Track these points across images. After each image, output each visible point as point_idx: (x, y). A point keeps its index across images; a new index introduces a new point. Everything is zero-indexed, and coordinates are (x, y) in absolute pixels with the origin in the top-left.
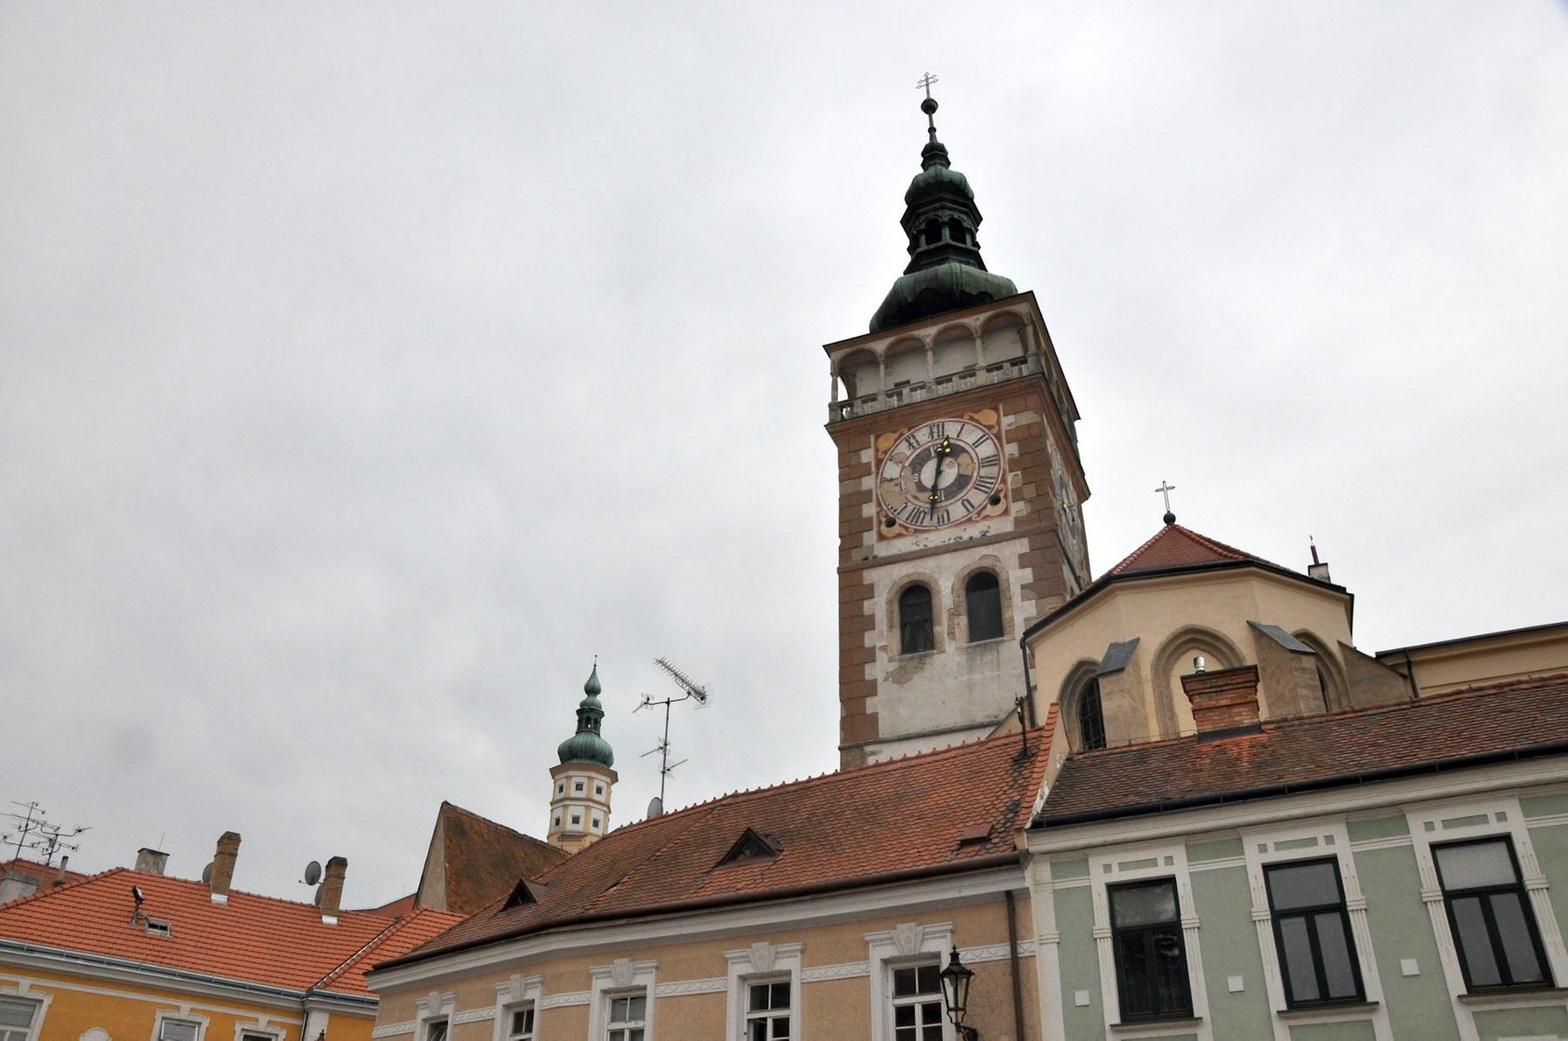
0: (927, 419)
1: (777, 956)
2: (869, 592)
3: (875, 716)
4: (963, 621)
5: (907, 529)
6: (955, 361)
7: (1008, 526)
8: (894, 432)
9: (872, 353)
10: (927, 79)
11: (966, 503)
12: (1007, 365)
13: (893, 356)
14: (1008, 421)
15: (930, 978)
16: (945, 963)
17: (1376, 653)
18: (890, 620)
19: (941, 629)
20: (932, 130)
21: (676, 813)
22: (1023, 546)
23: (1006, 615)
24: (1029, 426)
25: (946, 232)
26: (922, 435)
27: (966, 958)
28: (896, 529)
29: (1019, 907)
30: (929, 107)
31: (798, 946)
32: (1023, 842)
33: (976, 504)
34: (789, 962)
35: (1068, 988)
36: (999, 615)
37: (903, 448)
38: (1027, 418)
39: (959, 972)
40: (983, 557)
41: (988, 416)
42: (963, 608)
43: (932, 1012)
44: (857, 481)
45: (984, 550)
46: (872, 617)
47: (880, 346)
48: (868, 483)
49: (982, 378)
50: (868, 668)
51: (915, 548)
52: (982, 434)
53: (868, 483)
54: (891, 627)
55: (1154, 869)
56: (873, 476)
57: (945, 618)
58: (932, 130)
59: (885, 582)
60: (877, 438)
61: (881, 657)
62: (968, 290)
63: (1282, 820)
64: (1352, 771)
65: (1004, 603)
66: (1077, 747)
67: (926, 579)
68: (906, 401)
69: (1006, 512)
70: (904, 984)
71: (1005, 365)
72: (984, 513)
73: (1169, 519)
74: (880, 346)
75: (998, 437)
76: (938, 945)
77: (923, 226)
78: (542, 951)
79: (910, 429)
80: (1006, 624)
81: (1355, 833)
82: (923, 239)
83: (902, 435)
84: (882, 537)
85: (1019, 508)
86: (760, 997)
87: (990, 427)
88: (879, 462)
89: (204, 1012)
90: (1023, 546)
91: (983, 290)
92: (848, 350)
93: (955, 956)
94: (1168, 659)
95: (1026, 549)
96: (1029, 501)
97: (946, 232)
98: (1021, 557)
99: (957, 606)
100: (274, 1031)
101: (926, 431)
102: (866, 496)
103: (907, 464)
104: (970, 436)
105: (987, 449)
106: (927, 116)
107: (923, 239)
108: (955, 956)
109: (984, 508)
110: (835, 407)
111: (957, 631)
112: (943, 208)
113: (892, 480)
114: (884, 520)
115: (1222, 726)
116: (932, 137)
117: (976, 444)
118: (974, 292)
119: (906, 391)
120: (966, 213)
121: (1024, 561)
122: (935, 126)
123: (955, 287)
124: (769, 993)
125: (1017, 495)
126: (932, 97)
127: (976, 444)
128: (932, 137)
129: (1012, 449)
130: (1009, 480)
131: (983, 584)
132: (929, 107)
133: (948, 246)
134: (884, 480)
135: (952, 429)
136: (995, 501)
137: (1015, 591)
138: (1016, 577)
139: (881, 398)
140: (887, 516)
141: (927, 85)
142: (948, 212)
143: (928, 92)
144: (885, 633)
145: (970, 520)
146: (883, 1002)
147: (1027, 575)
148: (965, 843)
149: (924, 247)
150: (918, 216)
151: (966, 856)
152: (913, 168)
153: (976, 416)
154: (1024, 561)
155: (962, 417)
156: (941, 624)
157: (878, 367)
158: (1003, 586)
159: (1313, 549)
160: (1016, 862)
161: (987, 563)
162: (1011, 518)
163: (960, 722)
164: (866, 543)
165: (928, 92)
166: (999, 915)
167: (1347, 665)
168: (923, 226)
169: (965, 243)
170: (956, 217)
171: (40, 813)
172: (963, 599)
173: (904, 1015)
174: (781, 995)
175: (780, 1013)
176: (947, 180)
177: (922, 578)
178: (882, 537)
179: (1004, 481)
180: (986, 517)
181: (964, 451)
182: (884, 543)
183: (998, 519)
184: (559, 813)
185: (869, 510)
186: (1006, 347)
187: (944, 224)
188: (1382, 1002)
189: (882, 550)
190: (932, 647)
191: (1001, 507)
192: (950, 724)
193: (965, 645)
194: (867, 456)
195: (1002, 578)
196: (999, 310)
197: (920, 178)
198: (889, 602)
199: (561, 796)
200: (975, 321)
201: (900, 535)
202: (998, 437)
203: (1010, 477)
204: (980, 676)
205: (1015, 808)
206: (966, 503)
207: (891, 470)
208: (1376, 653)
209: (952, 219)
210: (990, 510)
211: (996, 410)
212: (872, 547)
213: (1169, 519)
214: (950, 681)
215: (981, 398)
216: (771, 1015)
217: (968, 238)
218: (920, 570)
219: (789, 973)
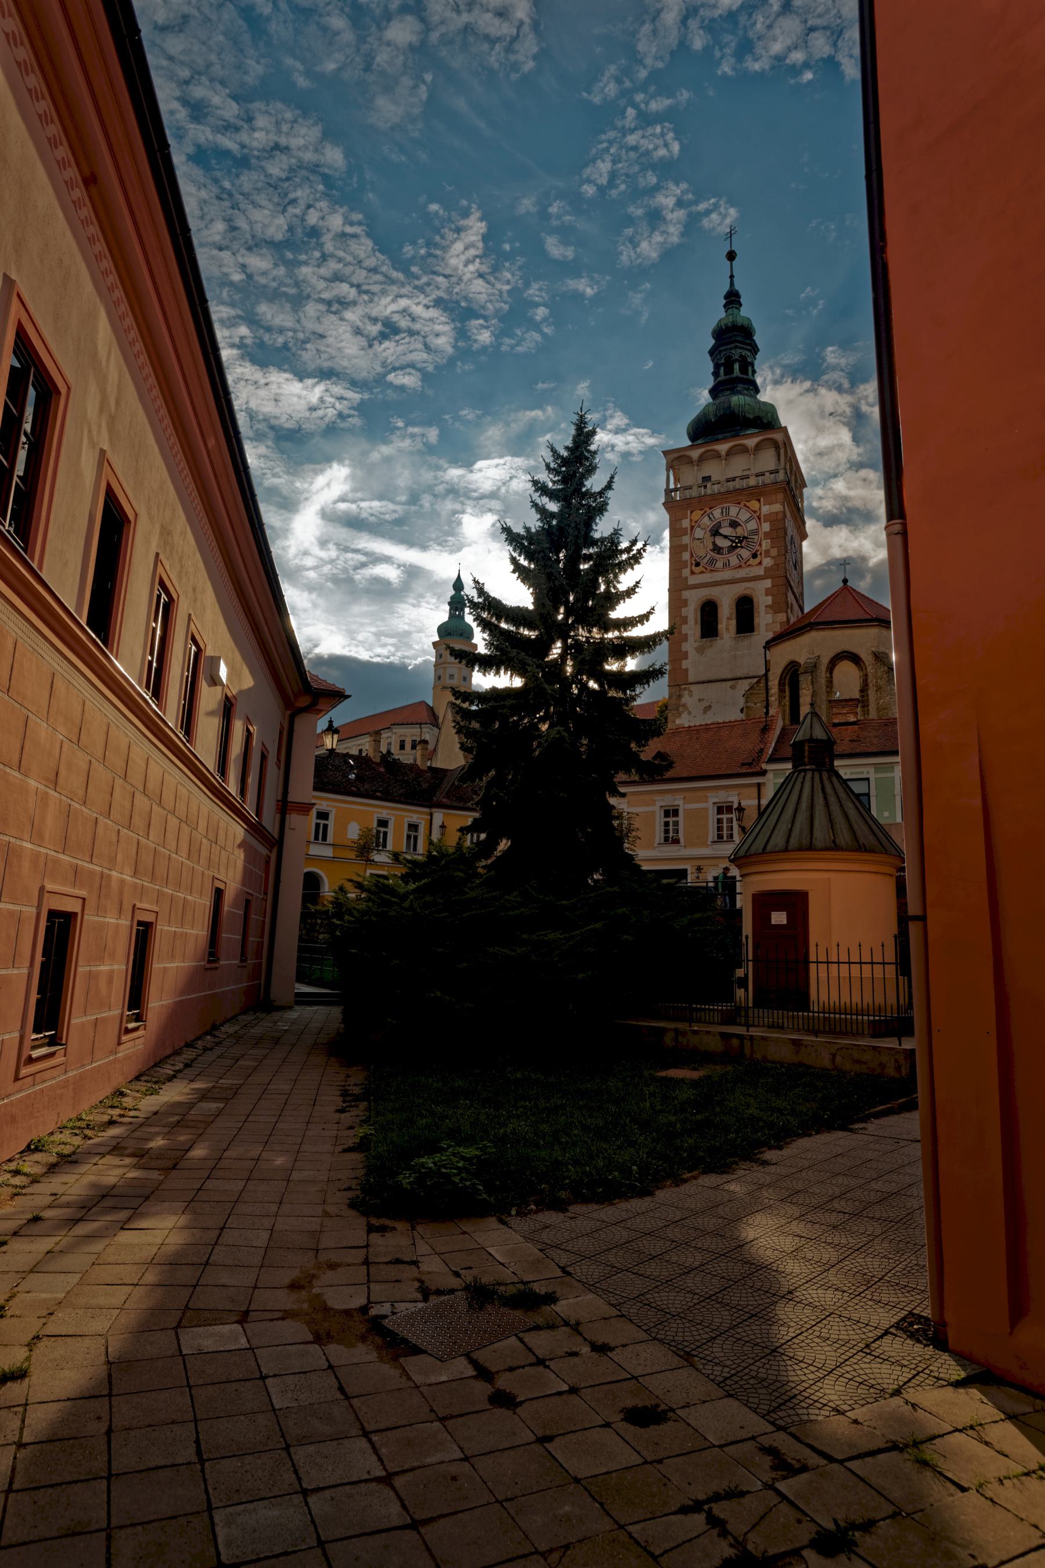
2: (685, 603)
3: (687, 670)
4: (734, 622)
6: (738, 466)
7: (760, 571)
9: (690, 457)
11: (739, 557)
12: (767, 474)
13: (702, 459)
14: (766, 509)
15: (729, 809)
16: (735, 806)
18: (696, 619)
19: (722, 626)
22: (768, 583)
23: (756, 621)
24: (777, 513)
25: (737, 366)
26: (717, 513)
27: (744, 804)
28: (700, 568)
29: (762, 788)
30: (731, 256)
32: (764, 766)
34: (679, 801)
36: (752, 620)
38: (777, 507)
39: (740, 809)
40: (748, 588)
41: (754, 505)
42: (734, 616)
43: (730, 820)
47: (695, 454)
48: (686, 540)
49: (752, 482)
50: (683, 644)
51: (710, 580)
53: (686, 540)
54: (696, 623)
59: (694, 598)
60: (691, 512)
61: (691, 639)
62: (748, 415)
65: (755, 615)
66: (787, 722)
68: (709, 492)
69: (760, 563)
70: (720, 810)
73: (845, 581)
74: (695, 454)
75: (759, 519)
76: (734, 799)
77: (723, 361)
80: (756, 626)
81: (876, 771)
82: (722, 369)
84: (692, 573)
85: (767, 562)
86: (667, 814)
87: (755, 512)
88: (692, 527)
90: (768, 583)
92: (676, 455)
93: (740, 803)
95: (769, 585)
96: (773, 558)
97: (737, 366)
98: (767, 589)
99: (731, 614)
101: (719, 511)
102: (684, 548)
104: (744, 516)
105: (752, 525)
108: (740, 803)
110: (668, 491)
112: (736, 347)
115: (842, 721)
116: (732, 284)
117: (747, 521)
119: (709, 485)
120: (750, 351)
121: (768, 592)
124: (671, 812)
125: (767, 553)
127: (747, 521)
128: (732, 284)
129: (766, 527)
130: (764, 545)
131: (745, 609)
132: (731, 256)
133: (738, 377)
134: (694, 539)
135: (734, 511)
136: (755, 556)
138: (763, 601)
139: (695, 488)
142: (739, 351)
146: (712, 816)
147: (769, 600)
148: (743, 764)
149: (722, 377)
150: (720, 352)
151: (743, 770)
152: (717, 314)
154: (768, 592)
158: (755, 605)
160: (763, 773)
161: (748, 592)
162: (762, 567)
163: (729, 676)
164: (684, 575)
166: (755, 790)
167: (665, 1078)
168: (723, 361)
172: (734, 611)
174: (676, 813)
175: (675, 819)
178: (692, 573)
179: (760, 545)
181: (739, 525)
182: (694, 576)
184: (441, 672)
185: (686, 556)
186: (767, 460)
187: (736, 360)
189: (693, 580)
190: (717, 635)
191: (757, 560)
192: (724, 677)
194: (686, 523)
195: (755, 601)
197: (722, 323)
198: (696, 610)
199: (442, 660)
201: (702, 572)
202: (759, 519)
203: (764, 543)
205: (761, 751)
206: (739, 557)
207: (699, 533)
209: (741, 356)
210: (752, 561)
211: (759, 501)
212: (686, 578)
213: (845, 581)
216: (671, 820)
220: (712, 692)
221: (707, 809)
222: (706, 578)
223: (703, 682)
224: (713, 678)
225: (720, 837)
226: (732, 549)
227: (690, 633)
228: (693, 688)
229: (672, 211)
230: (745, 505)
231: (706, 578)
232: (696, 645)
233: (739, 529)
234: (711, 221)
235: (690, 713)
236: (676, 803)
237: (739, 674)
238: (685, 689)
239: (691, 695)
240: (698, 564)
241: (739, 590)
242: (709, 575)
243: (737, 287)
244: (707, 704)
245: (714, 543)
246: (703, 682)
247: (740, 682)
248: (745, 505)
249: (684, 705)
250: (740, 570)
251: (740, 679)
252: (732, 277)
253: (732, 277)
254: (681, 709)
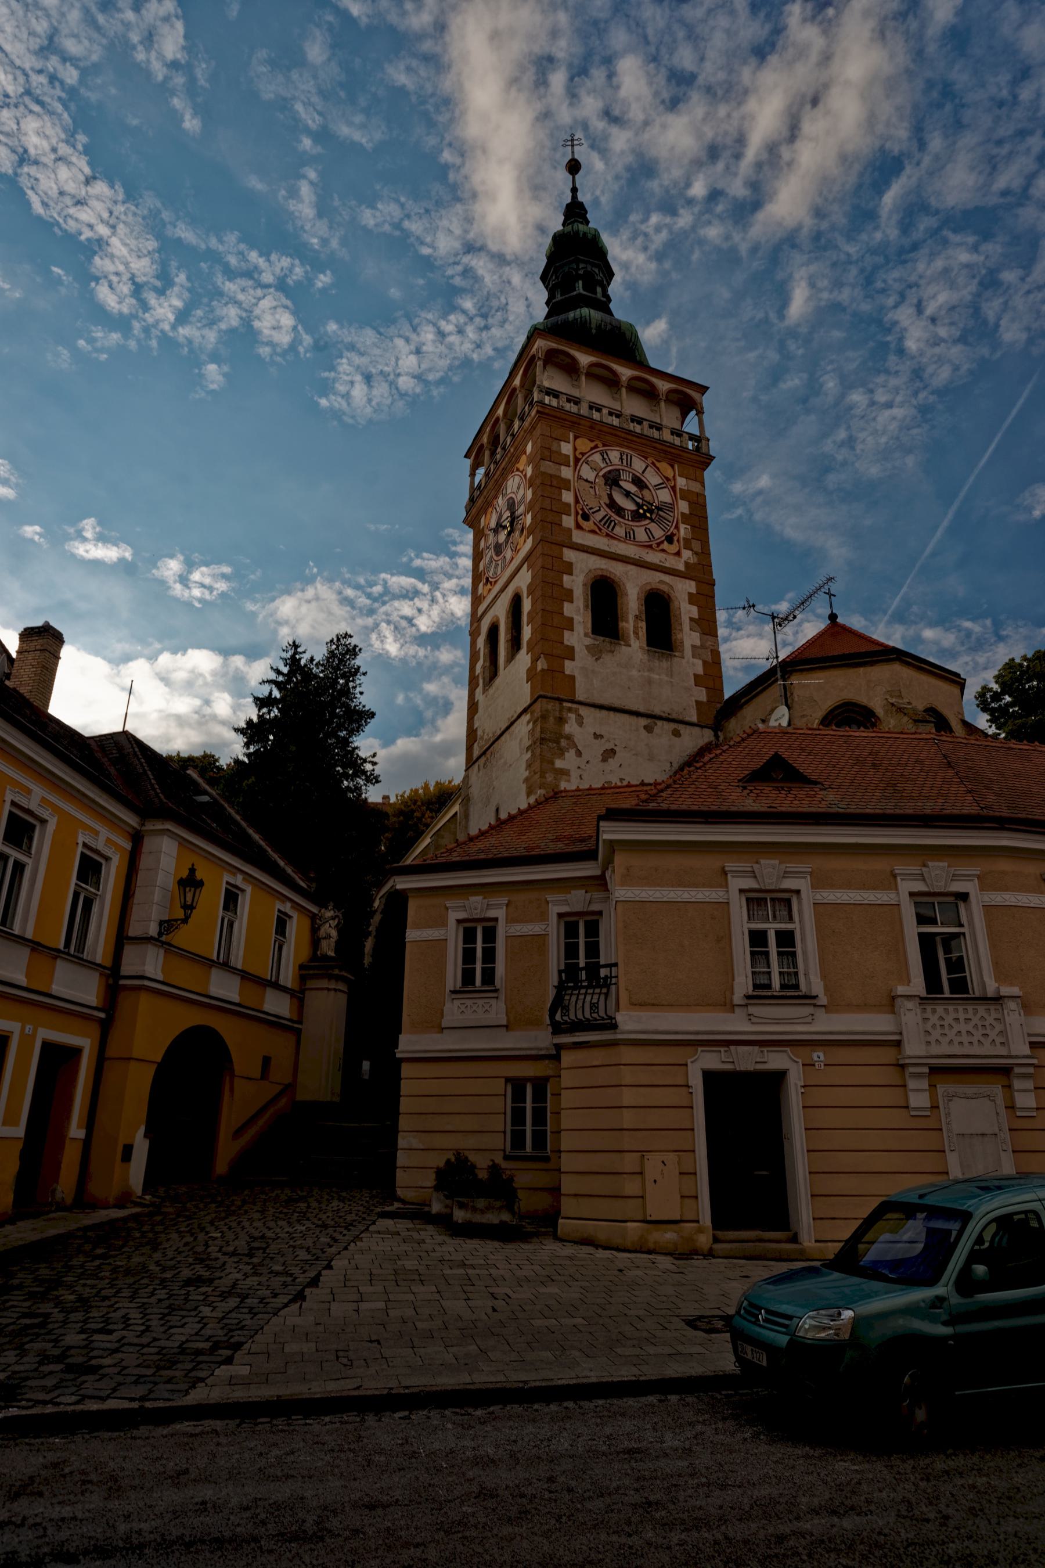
0: (621, 446)
1: (489, 907)
3: (572, 678)
5: (600, 529)
8: (592, 441)
10: (573, 140)
12: (564, 398)
18: (586, 600)
20: (574, 190)
31: (505, 900)
33: (657, 536)
37: (597, 458)
40: (661, 582)
44: (557, 466)
45: (666, 578)
46: (571, 591)
51: (606, 548)
52: (661, 481)
54: (586, 607)
56: (571, 469)
57: (631, 619)
58: (574, 190)
67: (616, 579)
71: (561, 396)
72: (661, 547)
73: (833, 617)
79: (604, 445)
83: (596, 447)
87: (668, 479)
89: (56, 809)
100: (45, 814)
103: (601, 474)
104: (652, 478)
109: (662, 542)
111: (640, 634)
113: (587, 481)
114: (580, 512)
122: (577, 186)
126: (576, 157)
132: (574, 167)
135: (638, 465)
136: (670, 539)
137: (686, 625)
140: (582, 509)
141: (573, 146)
143: (573, 152)
144: (582, 610)
145: (650, 547)
146: (741, 924)
153: (658, 464)
155: (646, 458)
156: (627, 621)
157: (658, 403)
165: (573, 152)
169: (595, 293)
173: (758, 938)
177: (612, 577)
180: (663, 551)
183: (672, 557)
191: (673, 548)
193: (645, 645)
196: (680, 388)
200: (625, 373)
204: (657, 677)
213: (833, 617)
214: (634, 673)
215: (665, 452)
217: (599, 290)
218: (611, 569)
219: (496, 920)
220: (617, 728)
221: (543, 937)
222: (599, 542)
223: (601, 707)
224: (617, 703)
225: (468, 977)
226: (637, 516)
227: (578, 619)
228: (583, 711)
229: (170, 306)
230: (653, 463)
231: (599, 542)
232: (588, 641)
233: (646, 492)
234: (296, 275)
235: (579, 753)
236: (492, 914)
237: (657, 711)
238: (570, 710)
239: (581, 724)
240: (586, 517)
241: (655, 579)
242: (605, 540)
244: (609, 746)
245: (610, 497)
246: (601, 707)
247: (659, 723)
248: (653, 463)
249: (569, 738)
250: (650, 551)
251: (660, 718)
254: (563, 743)
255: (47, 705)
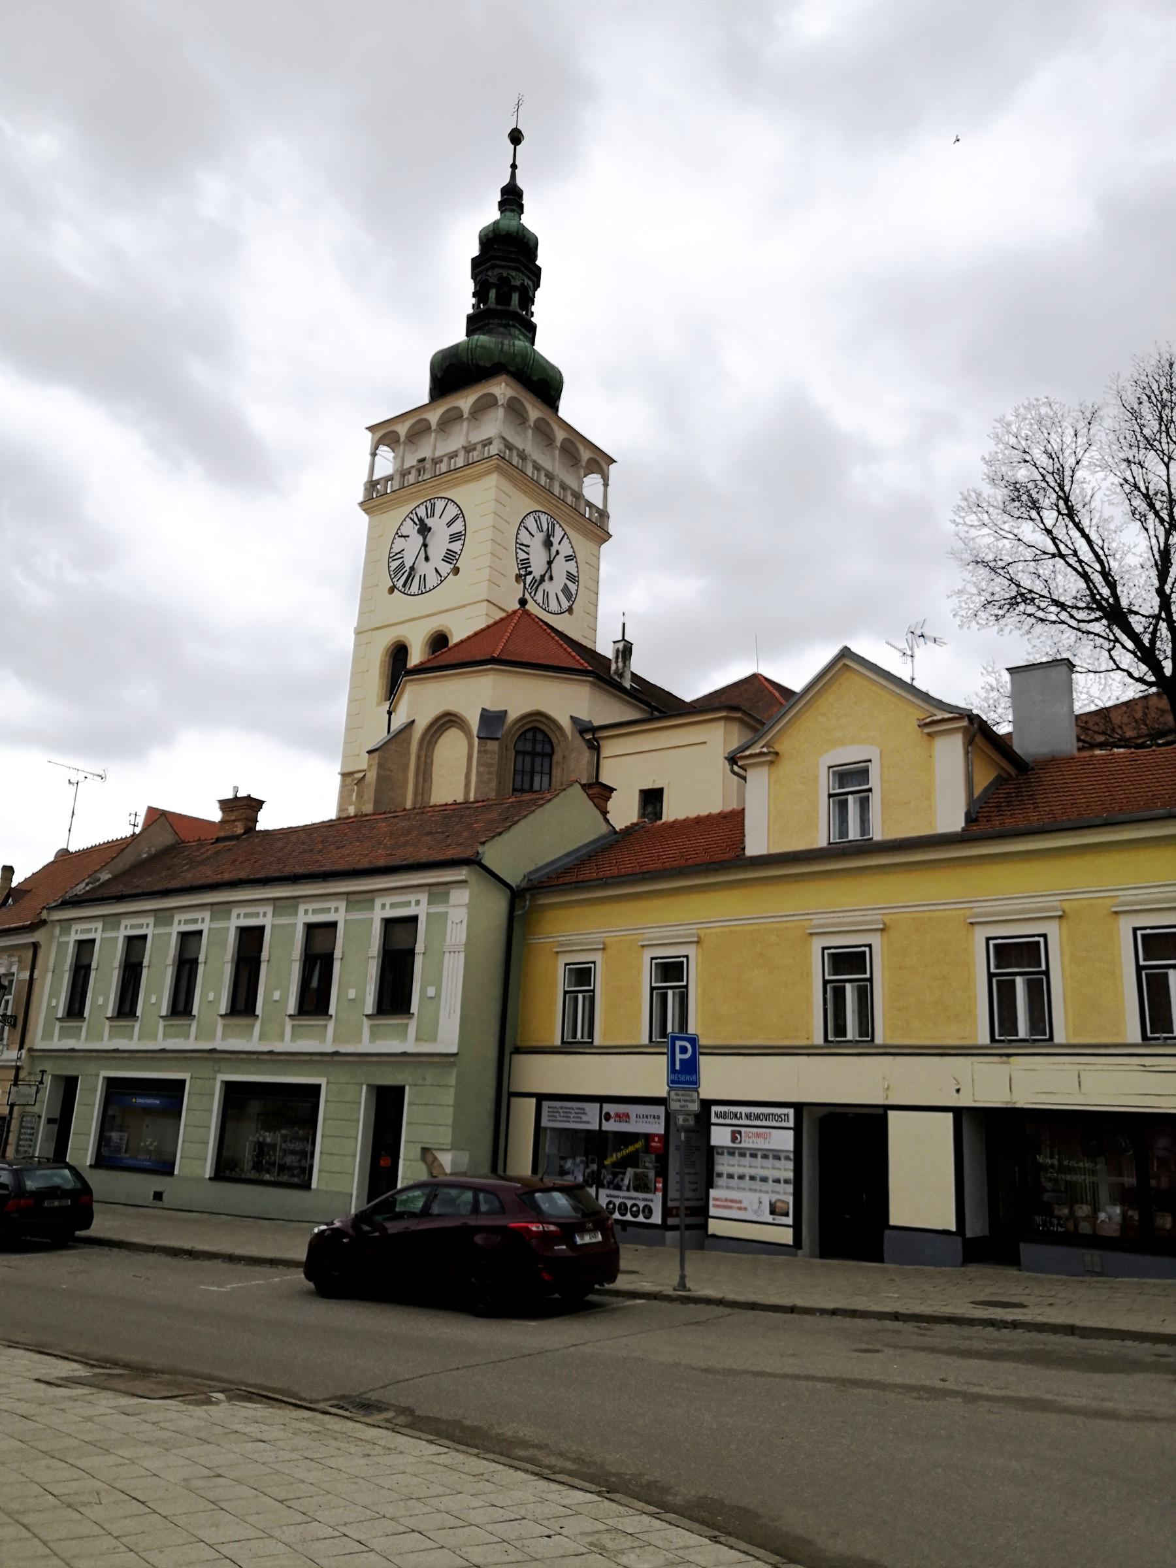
17: (224, 804)
21: (676, 822)
30: (516, 137)
35: (50, 997)
55: (140, 930)
62: (482, 363)
63: (185, 907)
64: (364, 864)
74: (434, 417)
78: (170, 978)
82: (492, 294)
91: (496, 360)
94: (427, 750)
97: (515, 297)
106: (513, 146)
107: (492, 294)
118: (488, 365)
123: (470, 362)
132: (516, 137)
145: (1089, 429)
159: (624, 624)
170: (505, 275)
171: (1097, 657)
176: (505, 233)
188: (260, 1016)
208: (224, 804)
209: (522, 284)
243: (520, 183)
252: (514, 166)
253: (514, 166)
255: (25, 980)
